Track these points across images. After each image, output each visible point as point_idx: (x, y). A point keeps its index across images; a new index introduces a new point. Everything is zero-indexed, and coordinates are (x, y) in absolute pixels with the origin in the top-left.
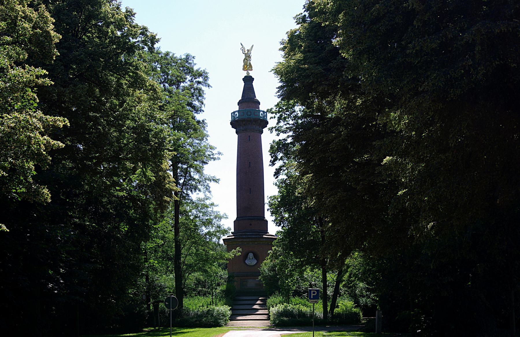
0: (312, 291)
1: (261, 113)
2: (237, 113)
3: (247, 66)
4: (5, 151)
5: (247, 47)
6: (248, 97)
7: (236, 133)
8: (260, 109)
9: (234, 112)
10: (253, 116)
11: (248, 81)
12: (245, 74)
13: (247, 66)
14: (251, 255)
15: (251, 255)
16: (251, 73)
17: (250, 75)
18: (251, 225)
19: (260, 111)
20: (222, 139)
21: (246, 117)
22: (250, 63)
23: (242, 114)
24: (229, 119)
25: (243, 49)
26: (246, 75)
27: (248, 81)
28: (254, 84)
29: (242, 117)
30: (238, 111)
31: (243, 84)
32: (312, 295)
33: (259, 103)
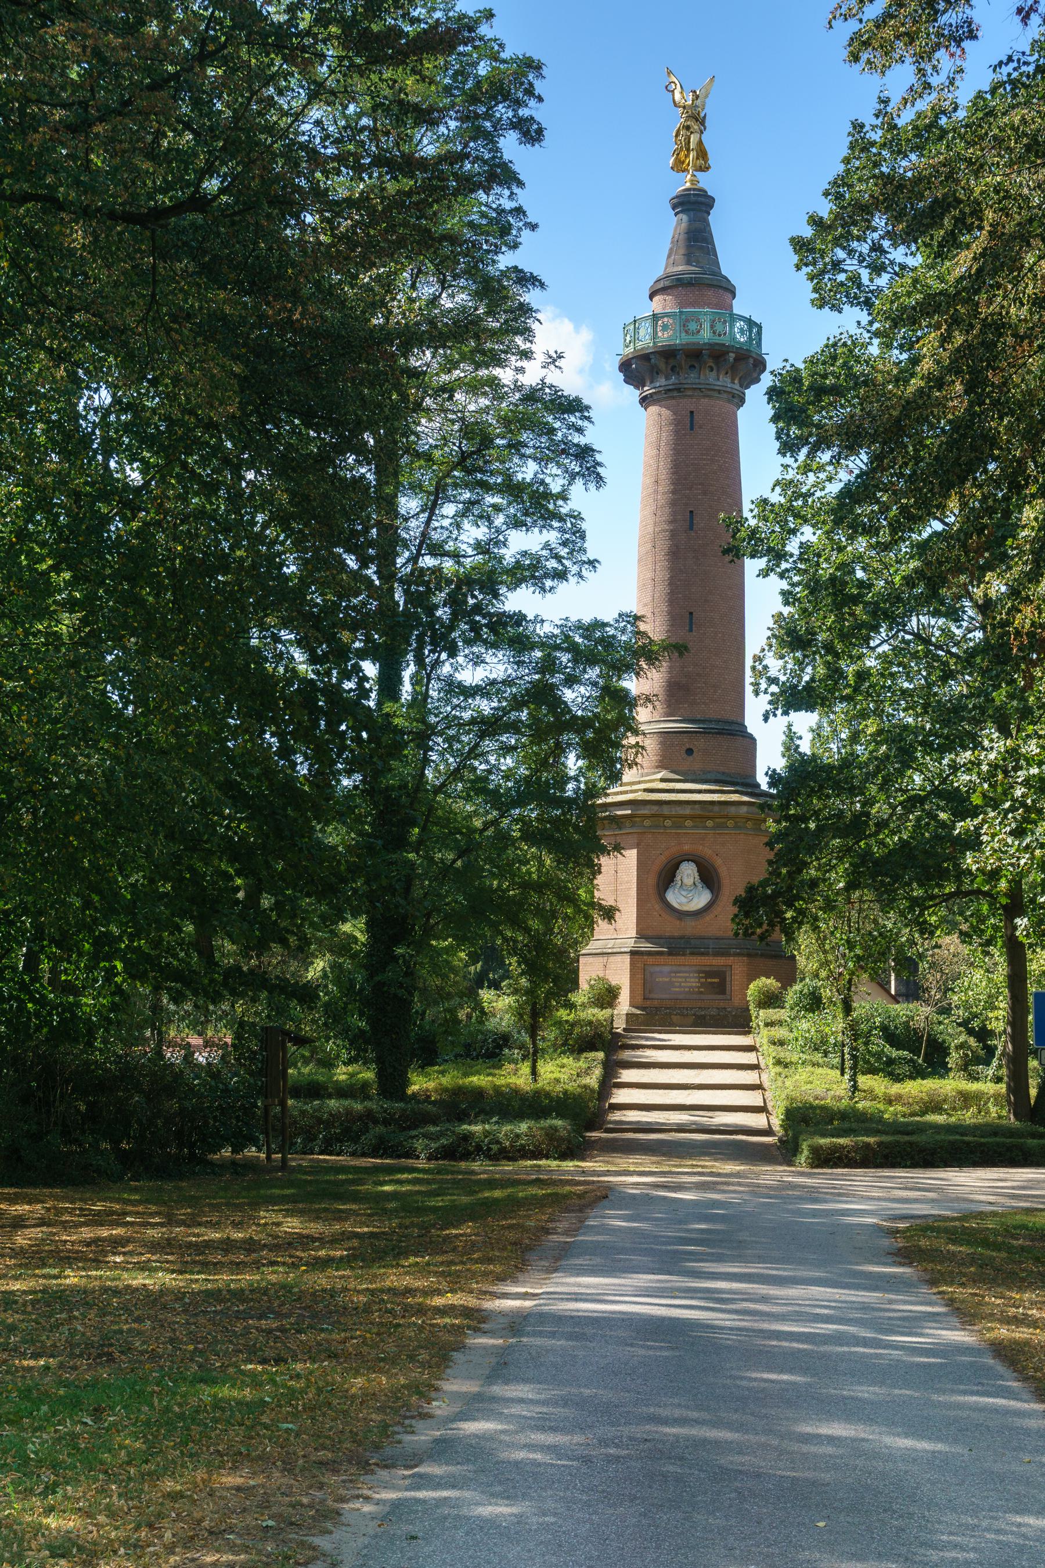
11: (695, 206)
14: (688, 872)
15: (688, 872)
16: (706, 181)
17: (701, 185)
24: (617, 361)
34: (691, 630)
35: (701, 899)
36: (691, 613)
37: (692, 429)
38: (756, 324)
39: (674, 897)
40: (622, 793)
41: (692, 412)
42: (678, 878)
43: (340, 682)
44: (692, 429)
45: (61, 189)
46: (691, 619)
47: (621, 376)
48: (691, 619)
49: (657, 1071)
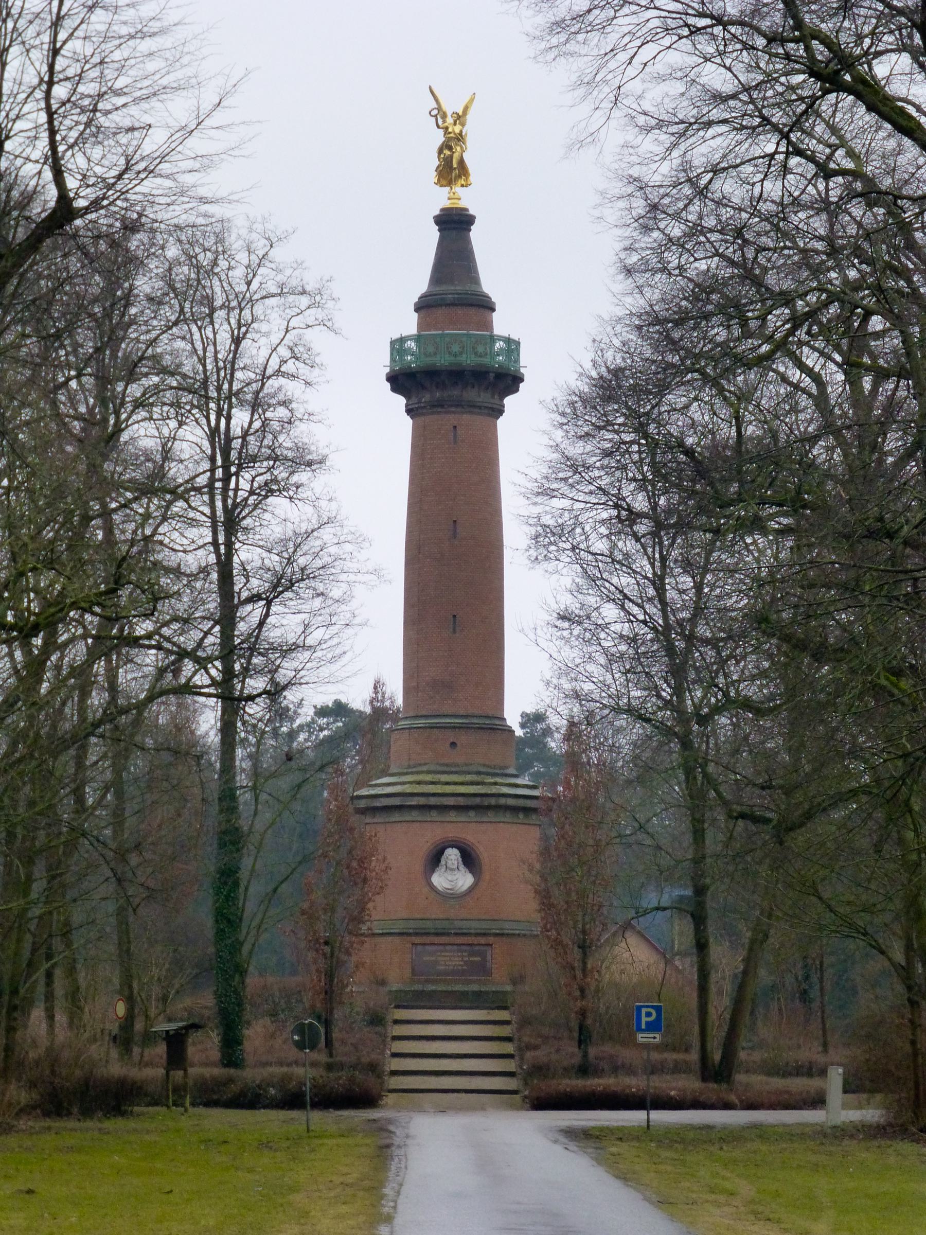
0: (644, 1011)
1: (499, 345)
2: (412, 344)
3: (451, 170)
4: (340, 1078)
5: (452, 106)
6: (454, 293)
7: (409, 411)
8: (497, 331)
9: (402, 340)
10: (468, 360)
11: (454, 224)
12: (440, 198)
13: (451, 170)
14: (452, 855)
15: (452, 855)
16: (467, 198)
17: (462, 204)
18: (453, 744)
19: (493, 339)
20: (358, 464)
21: (443, 360)
22: (461, 162)
23: (431, 349)
24: (382, 363)
25: (439, 113)
26: (447, 204)
27: (454, 224)
28: (476, 234)
29: (429, 360)
30: (418, 338)
31: (434, 234)
32: (644, 1019)
33: (489, 307)
34: (454, 631)
35: (464, 880)
36: (455, 616)
37: (455, 442)
38: (514, 341)
39: (439, 880)
40: (389, 784)
41: (455, 427)
42: (443, 862)
43: (917, 229)
44: (455, 442)
45: (861, 739)
46: (455, 623)
47: (388, 385)
48: (455, 623)
49: (425, 1042)
